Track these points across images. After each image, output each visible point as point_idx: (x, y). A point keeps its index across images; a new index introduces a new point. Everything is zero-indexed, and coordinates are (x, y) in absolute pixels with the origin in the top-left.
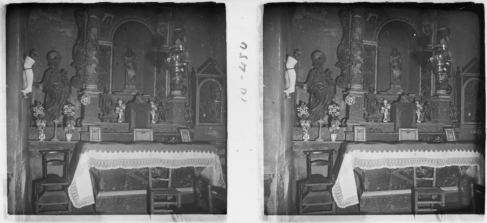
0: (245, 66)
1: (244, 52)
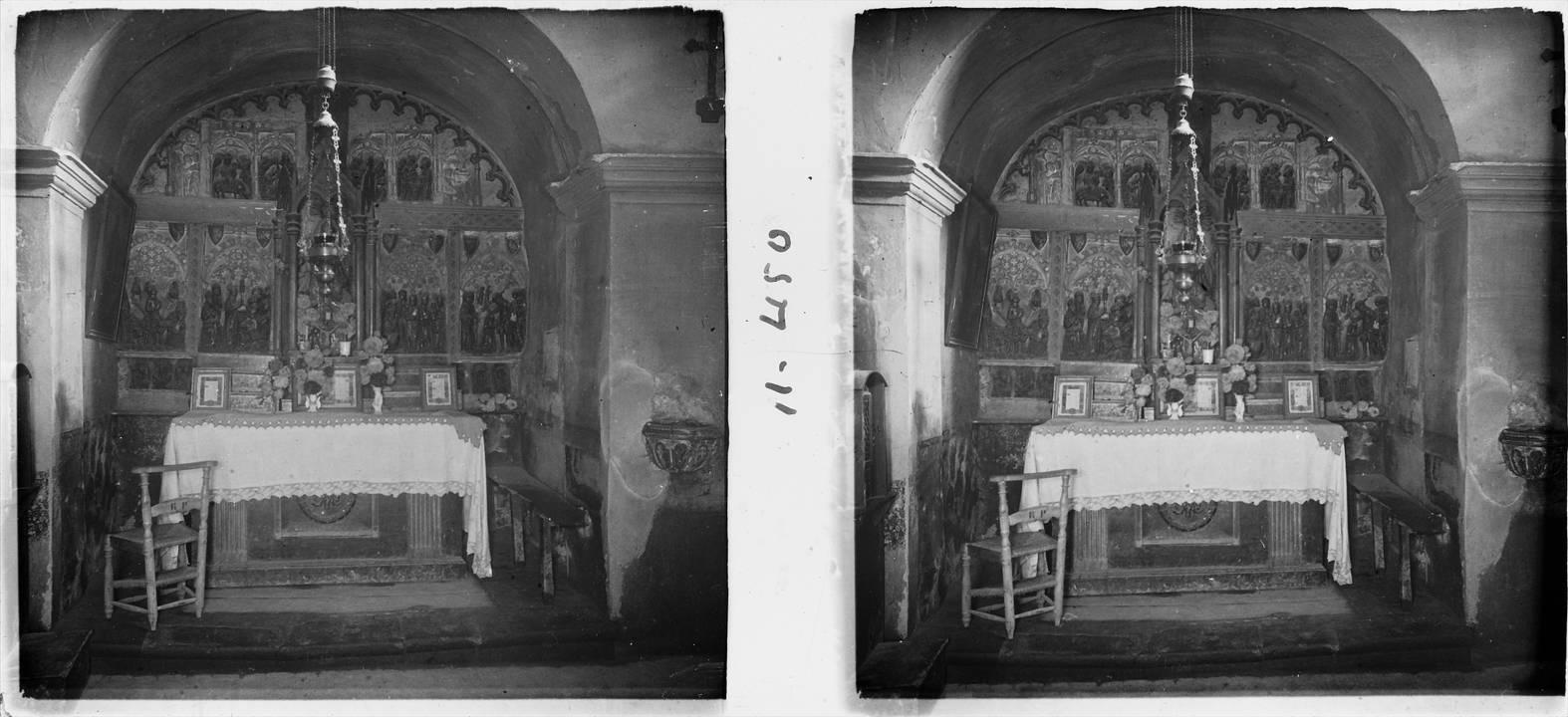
0: (782, 306)
1: (780, 263)
